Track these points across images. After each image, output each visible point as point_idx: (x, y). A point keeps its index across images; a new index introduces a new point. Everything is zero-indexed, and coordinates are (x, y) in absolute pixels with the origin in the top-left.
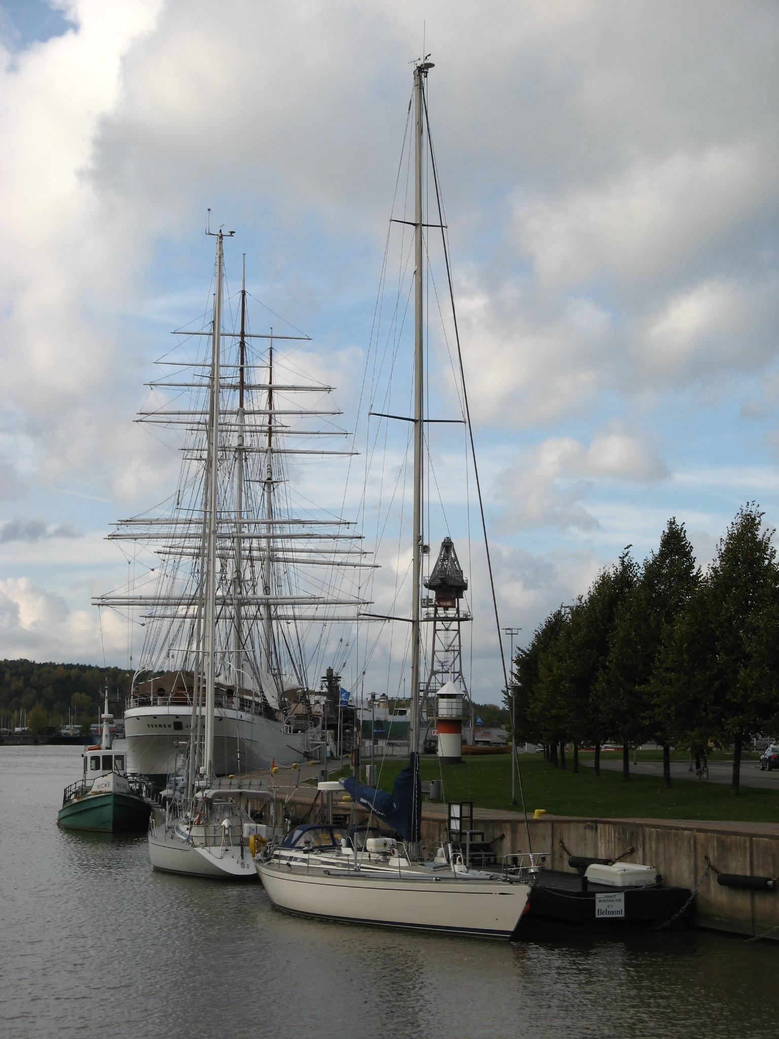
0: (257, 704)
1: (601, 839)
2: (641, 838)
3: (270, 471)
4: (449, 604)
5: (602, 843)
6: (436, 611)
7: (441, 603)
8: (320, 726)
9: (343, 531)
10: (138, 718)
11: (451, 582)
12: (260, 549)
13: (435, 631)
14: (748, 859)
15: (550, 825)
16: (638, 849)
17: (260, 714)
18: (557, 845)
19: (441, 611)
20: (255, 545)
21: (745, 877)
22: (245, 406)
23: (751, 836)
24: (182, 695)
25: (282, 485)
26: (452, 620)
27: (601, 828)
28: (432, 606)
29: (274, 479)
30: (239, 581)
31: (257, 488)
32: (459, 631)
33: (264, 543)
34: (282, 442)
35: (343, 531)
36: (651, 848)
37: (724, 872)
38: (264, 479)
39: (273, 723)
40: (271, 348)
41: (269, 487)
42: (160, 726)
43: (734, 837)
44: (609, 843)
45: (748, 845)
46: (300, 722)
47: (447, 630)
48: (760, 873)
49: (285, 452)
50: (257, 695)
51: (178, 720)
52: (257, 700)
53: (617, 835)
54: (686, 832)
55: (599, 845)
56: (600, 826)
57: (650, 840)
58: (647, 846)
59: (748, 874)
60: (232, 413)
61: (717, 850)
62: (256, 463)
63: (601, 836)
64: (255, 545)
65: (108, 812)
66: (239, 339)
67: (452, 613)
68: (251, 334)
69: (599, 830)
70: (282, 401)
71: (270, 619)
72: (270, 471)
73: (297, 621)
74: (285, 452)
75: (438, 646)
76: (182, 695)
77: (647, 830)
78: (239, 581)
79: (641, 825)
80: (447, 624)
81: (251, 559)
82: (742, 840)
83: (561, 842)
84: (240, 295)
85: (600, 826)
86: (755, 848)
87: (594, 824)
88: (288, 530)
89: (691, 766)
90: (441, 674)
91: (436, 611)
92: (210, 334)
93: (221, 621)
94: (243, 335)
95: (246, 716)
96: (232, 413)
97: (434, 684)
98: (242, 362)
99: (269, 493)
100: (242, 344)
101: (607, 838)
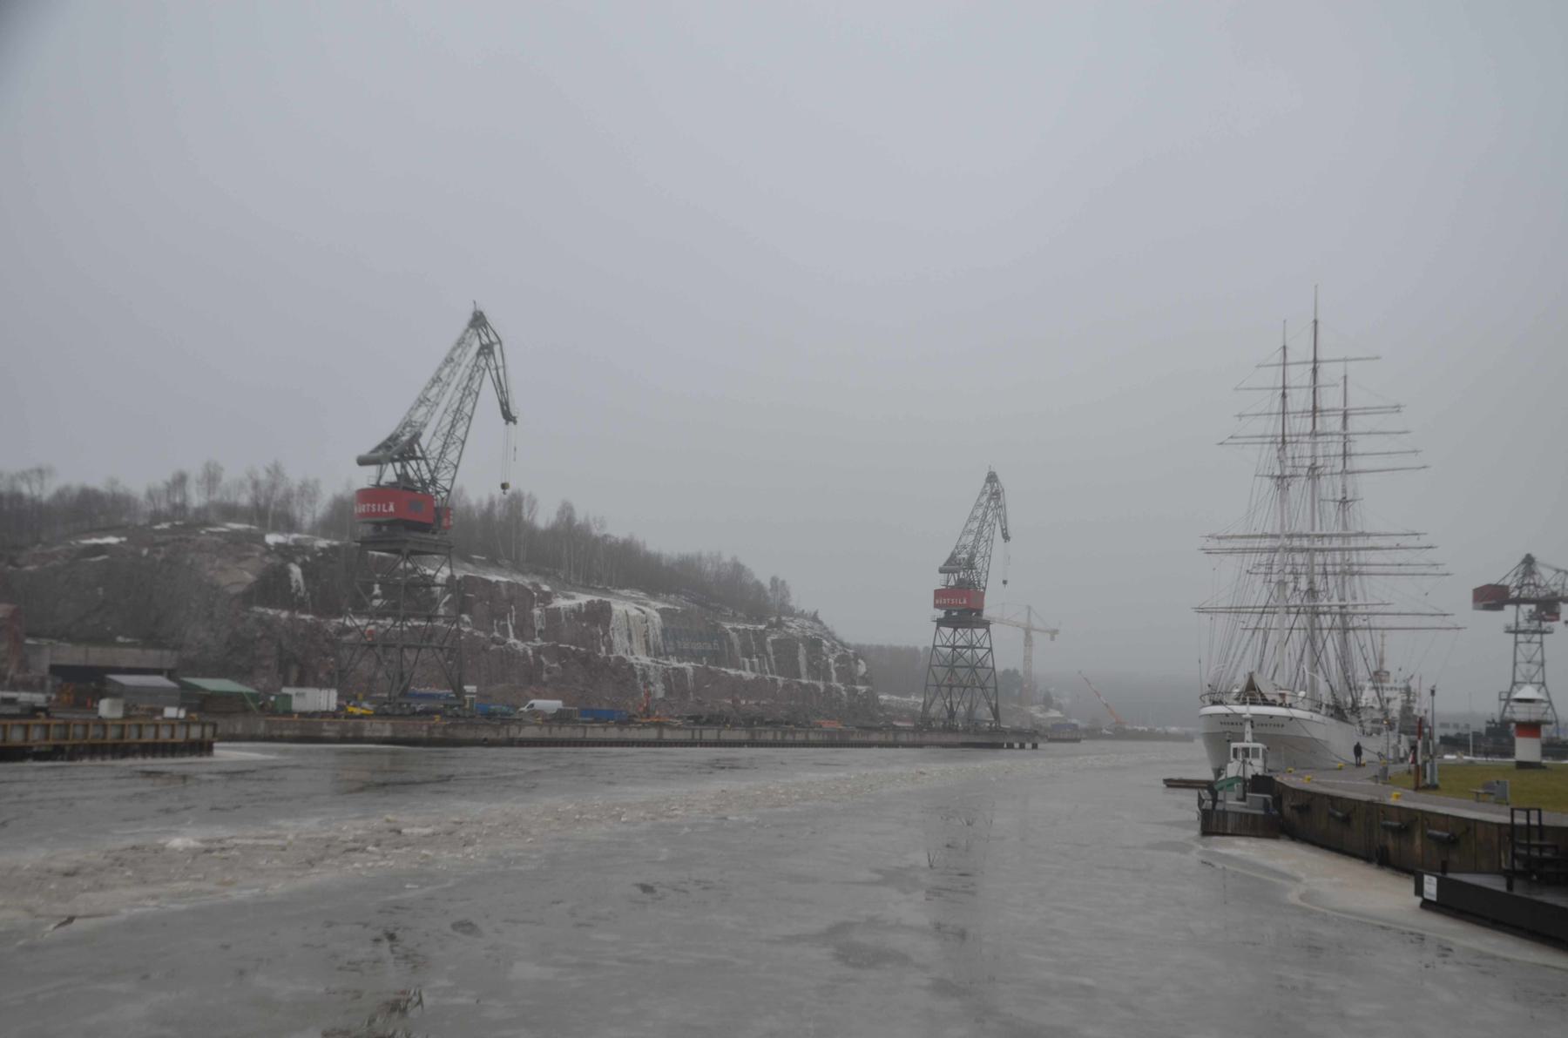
3: (1344, 491)
8: (1397, 730)
9: (1412, 541)
10: (1211, 715)
12: (1334, 565)
13: (1516, 643)
17: (1332, 716)
20: (1329, 560)
22: (1347, 468)
25: (1356, 504)
26: (1534, 632)
29: (1348, 499)
30: (1312, 592)
31: (1331, 508)
32: (1541, 643)
33: (1338, 557)
34: (1355, 463)
35: (1412, 541)
38: (1339, 497)
39: (1342, 724)
41: (1344, 506)
42: (1232, 724)
46: (1376, 726)
47: (1529, 642)
49: (1359, 472)
60: (1304, 435)
62: (1329, 487)
64: (1329, 560)
65: (1514, 765)
66: (1312, 366)
70: (1355, 424)
72: (1344, 491)
73: (1373, 631)
74: (1359, 472)
75: (1520, 658)
78: (1312, 592)
80: (1529, 636)
81: (1325, 574)
84: (1313, 325)
88: (1360, 542)
89: (1059, 708)
93: (1294, 631)
94: (1315, 361)
95: (1316, 717)
96: (1304, 435)
97: (1339, 461)
99: (1344, 511)
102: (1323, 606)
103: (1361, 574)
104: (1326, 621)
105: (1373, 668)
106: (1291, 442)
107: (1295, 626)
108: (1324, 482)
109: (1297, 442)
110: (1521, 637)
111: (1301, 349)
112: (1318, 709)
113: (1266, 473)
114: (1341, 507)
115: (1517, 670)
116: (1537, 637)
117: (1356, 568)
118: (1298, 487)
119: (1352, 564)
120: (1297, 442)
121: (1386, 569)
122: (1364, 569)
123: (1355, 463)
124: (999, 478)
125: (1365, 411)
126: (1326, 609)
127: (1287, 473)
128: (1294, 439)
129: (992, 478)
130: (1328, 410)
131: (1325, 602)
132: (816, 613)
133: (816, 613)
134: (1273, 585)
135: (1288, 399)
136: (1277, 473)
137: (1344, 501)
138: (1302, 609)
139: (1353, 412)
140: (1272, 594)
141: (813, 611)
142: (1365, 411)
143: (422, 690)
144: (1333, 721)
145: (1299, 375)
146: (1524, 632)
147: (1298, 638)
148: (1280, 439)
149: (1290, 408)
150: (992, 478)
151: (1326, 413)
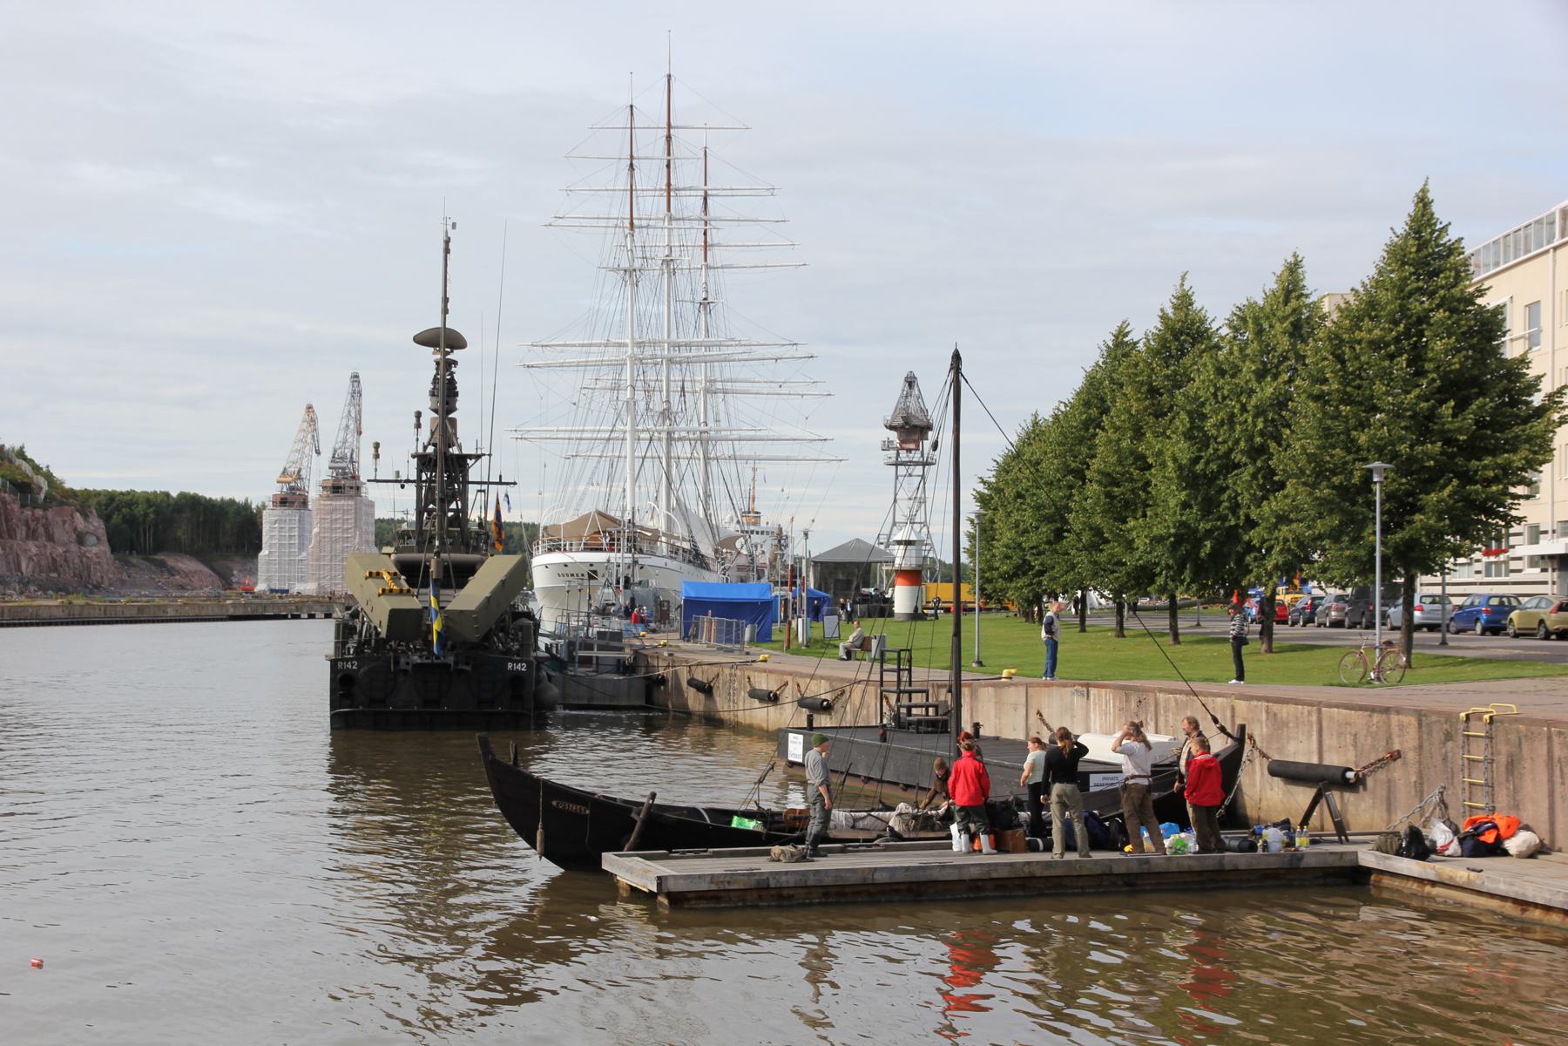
0: (684, 550)
1: (1094, 709)
2: (1152, 708)
4: (912, 446)
5: (1095, 715)
6: (898, 455)
7: (904, 445)
11: (916, 422)
14: (1315, 737)
15: (1022, 690)
16: (1147, 724)
17: (690, 561)
18: (1033, 718)
19: (903, 454)
21: (1309, 766)
23: (1319, 705)
24: (596, 539)
26: (917, 464)
27: (1094, 695)
28: (893, 448)
32: (923, 477)
36: (1167, 721)
37: (1276, 757)
40: (669, 76)
41: (705, 309)
43: (1292, 708)
44: (1106, 714)
45: (1314, 718)
48: (1333, 759)
50: (684, 539)
51: (592, 568)
52: (686, 545)
53: (1118, 704)
54: (1219, 700)
55: (1092, 716)
56: (1093, 691)
57: (1166, 711)
58: (1162, 719)
59: (1315, 761)
61: (1267, 725)
63: (1095, 705)
66: (665, 132)
67: (916, 456)
68: (678, 125)
69: (1092, 697)
71: (707, 459)
76: (596, 539)
77: (1161, 696)
79: (1153, 690)
82: (1306, 713)
83: (1039, 713)
85: (1093, 691)
86: (1325, 724)
87: (1085, 689)
90: (672, 131)
91: (898, 455)
92: (712, 245)
95: (672, 564)
98: (669, 154)
100: (669, 138)
101: (1104, 707)
102: (680, 431)
103: (725, 392)
104: (683, 449)
105: (742, 504)
106: (661, 190)
107: (649, 454)
108: (681, 280)
109: (647, 227)
110: (902, 470)
111: (651, 108)
112: (674, 555)
113: (611, 265)
114: (702, 309)
115: (897, 507)
116: (918, 470)
117: (719, 385)
118: (652, 277)
119: (715, 381)
120: (647, 227)
121: (777, 352)
122: (728, 386)
123: (716, 255)
124: (315, 409)
125: (732, 192)
126: (684, 434)
127: (637, 264)
128: (644, 223)
129: (310, 408)
130: (684, 189)
131: (683, 425)
132: (22, 448)
133: (22, 448)
134: (620, 403)
135: (636, 172)
136: (625, 264)
137: (705, 303)
138: (656, 434)
139: (714, 192)
140: (619, 415)
141: (17, 447)
142: (732, 192)
143: (512, 756)
144: (691, 568)
145: (650, 144)
146: (903, 464)
147: (653, 471)
148: (627, 223)
149: (638, 185)
150: (310, 408)
151: (683, 193)
